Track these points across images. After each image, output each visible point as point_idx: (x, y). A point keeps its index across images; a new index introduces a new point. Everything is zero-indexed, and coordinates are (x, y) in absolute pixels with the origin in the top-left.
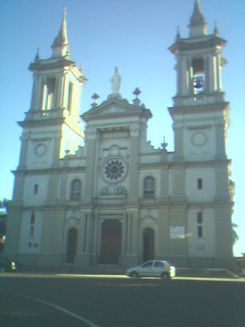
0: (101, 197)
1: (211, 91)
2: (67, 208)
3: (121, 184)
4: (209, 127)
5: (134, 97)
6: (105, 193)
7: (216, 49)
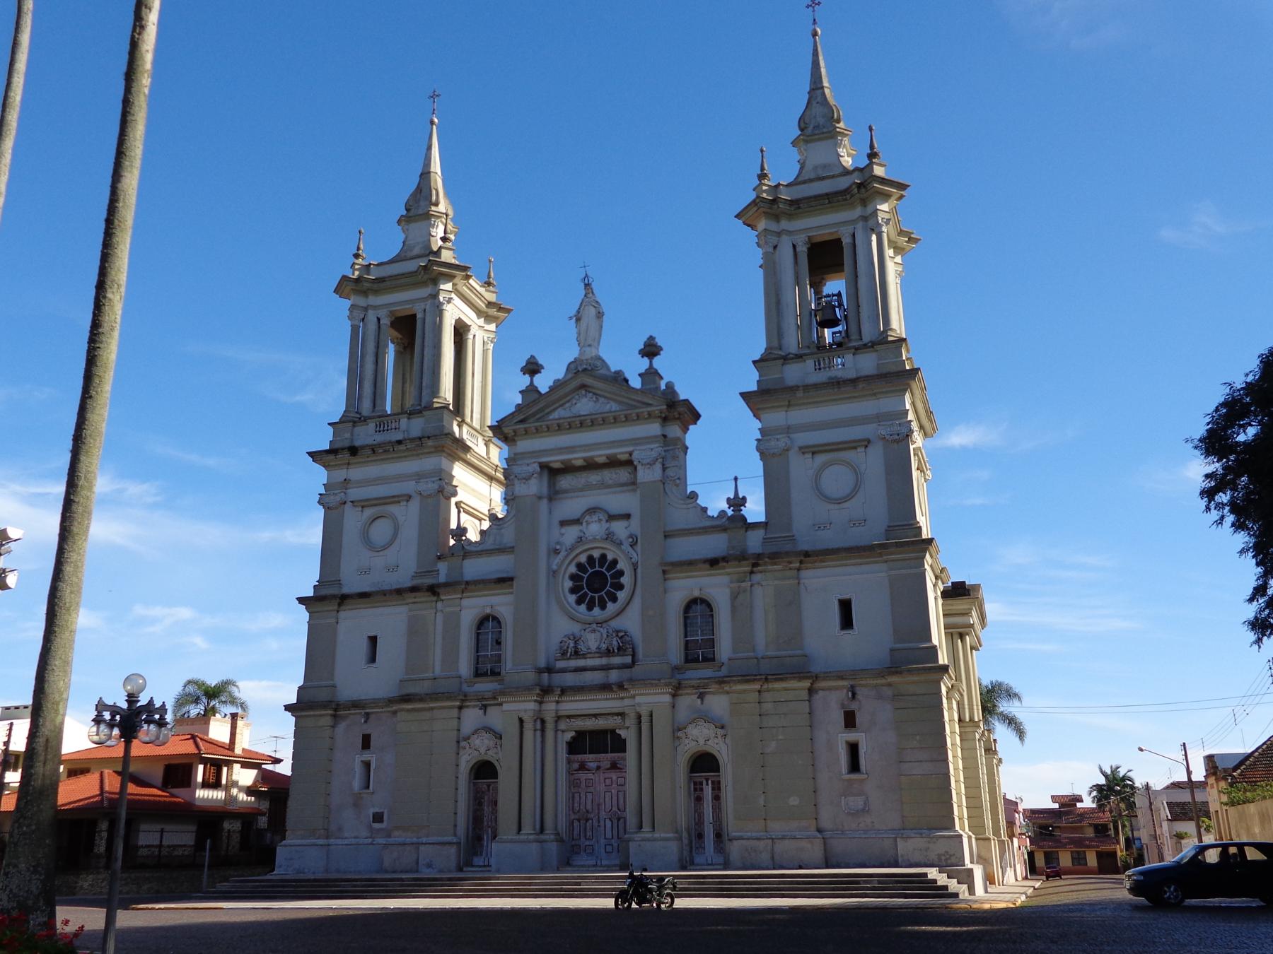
0: (561, 664)
2: (464, 701)
3: (615, 624)
5: (644, 364)
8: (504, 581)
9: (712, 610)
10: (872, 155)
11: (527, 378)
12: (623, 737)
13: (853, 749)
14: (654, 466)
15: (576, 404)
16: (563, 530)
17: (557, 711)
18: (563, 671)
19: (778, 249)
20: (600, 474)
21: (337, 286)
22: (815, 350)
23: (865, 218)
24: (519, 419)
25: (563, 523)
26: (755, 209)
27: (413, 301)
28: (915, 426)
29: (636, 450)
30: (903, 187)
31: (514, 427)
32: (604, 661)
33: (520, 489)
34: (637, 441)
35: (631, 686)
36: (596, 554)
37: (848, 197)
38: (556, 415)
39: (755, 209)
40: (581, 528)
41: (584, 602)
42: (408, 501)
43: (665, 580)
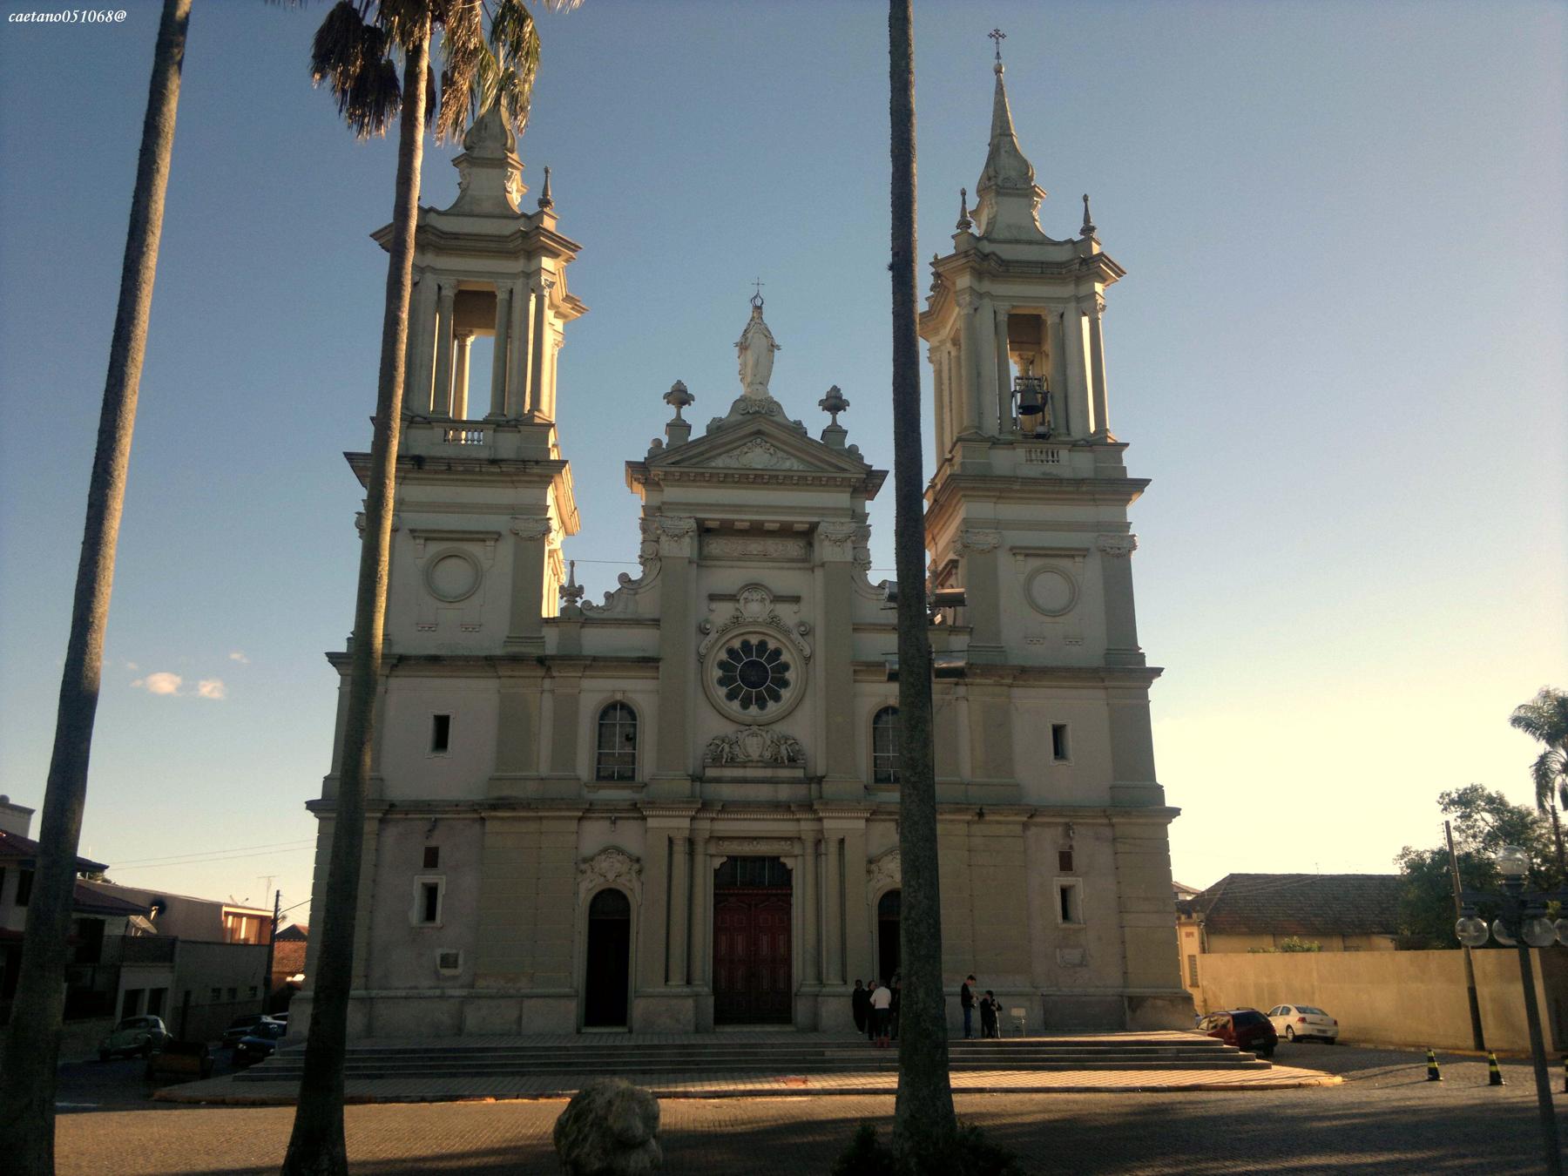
0: (711, 772)
1: (1076, 434)
2: (589, 811)
3: (781, 728)
4: (1084, 553)
5: (826, 419)
6: (721, 755)
7: (539, 270)
8: (648, 663)
9: (634, 719)
10: (544, 202)
11: (828, 415)
12: (789, 867)
13: (431, 892)
14: (845, 544)
15: (746, 453)
16: (714, 605)
17: (712, 831)
18: (718, 780)
19: (979, 311)
20: (762, 543)
21: (386, 228)
22: (1020, 438)
23: (1078, 299)
24: (673, 460)
25: (713, 598)
26: (964, 261)
27: (491, 274)
28: (555, 524)
29: (823, 521)
30: (574, 248)
31: (668, 469)
32: (768, 773)
33: (667, 547)
34: (823, 511)
35: (822, 807)
36: (754, 640)
37: (1064, 271)
38: (719, 462)
39: (964, 261)
40: (737, 605)
41: (736, 698)
42: (497, 540)
43: (855, 681)
